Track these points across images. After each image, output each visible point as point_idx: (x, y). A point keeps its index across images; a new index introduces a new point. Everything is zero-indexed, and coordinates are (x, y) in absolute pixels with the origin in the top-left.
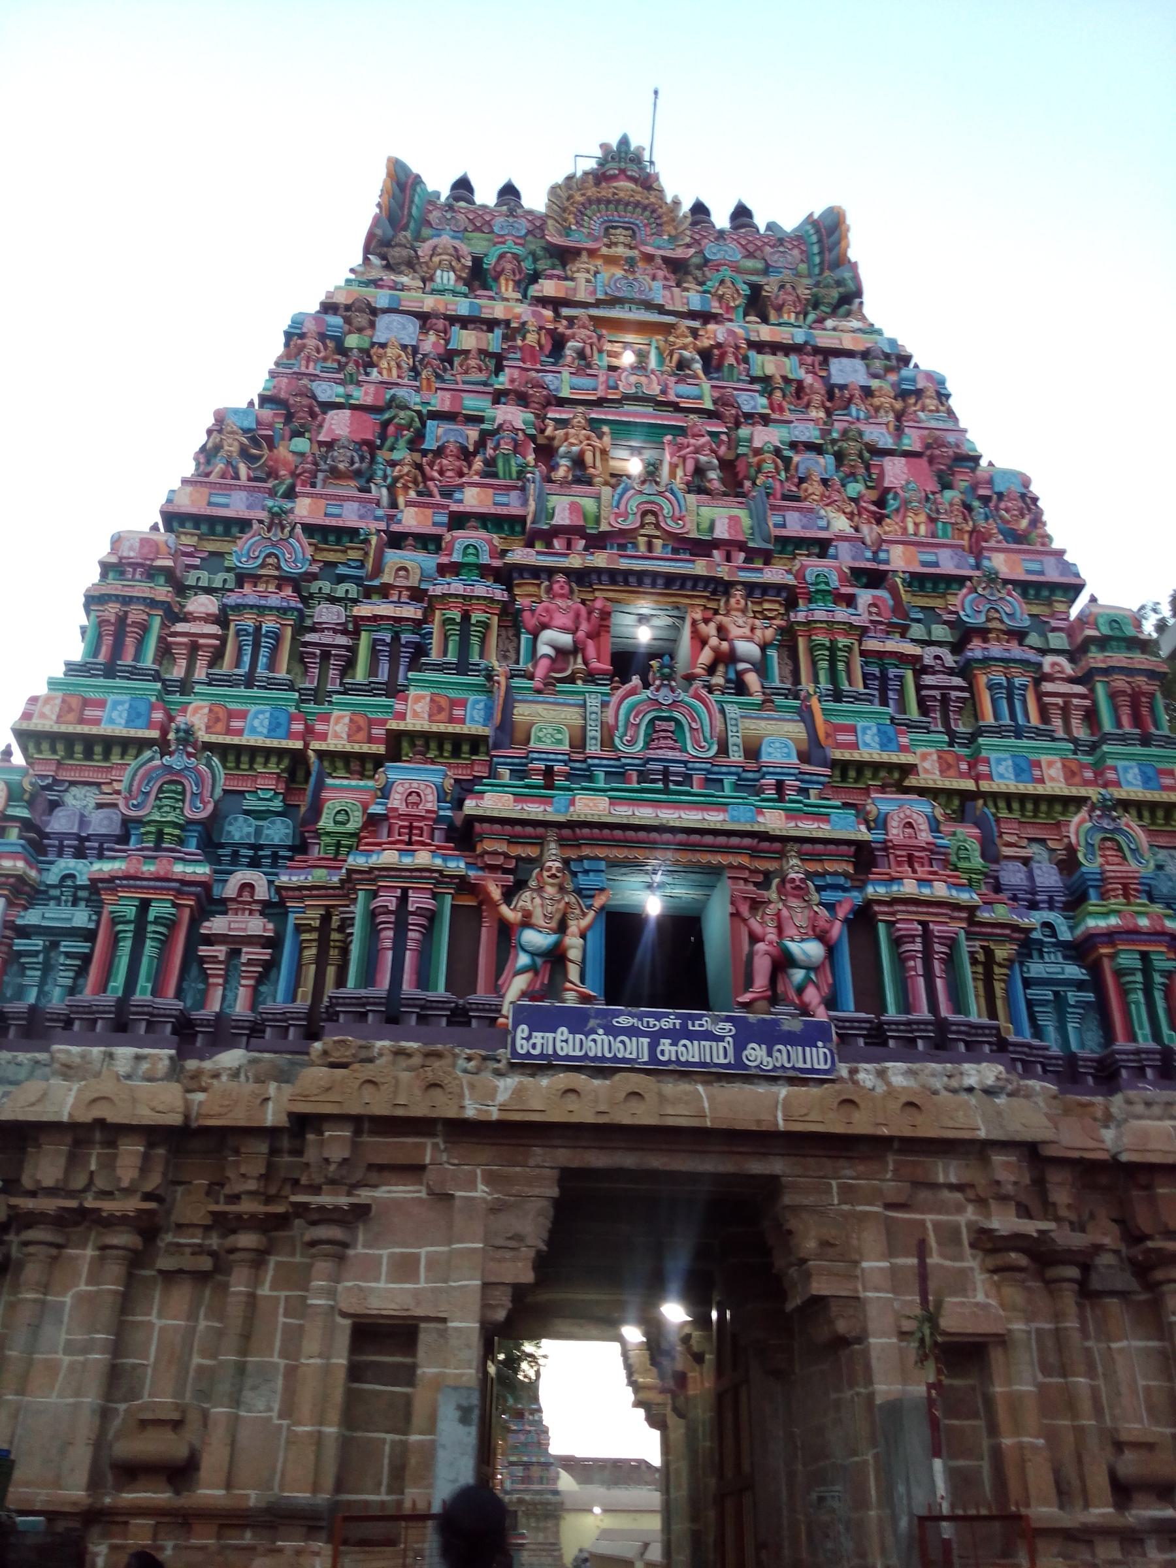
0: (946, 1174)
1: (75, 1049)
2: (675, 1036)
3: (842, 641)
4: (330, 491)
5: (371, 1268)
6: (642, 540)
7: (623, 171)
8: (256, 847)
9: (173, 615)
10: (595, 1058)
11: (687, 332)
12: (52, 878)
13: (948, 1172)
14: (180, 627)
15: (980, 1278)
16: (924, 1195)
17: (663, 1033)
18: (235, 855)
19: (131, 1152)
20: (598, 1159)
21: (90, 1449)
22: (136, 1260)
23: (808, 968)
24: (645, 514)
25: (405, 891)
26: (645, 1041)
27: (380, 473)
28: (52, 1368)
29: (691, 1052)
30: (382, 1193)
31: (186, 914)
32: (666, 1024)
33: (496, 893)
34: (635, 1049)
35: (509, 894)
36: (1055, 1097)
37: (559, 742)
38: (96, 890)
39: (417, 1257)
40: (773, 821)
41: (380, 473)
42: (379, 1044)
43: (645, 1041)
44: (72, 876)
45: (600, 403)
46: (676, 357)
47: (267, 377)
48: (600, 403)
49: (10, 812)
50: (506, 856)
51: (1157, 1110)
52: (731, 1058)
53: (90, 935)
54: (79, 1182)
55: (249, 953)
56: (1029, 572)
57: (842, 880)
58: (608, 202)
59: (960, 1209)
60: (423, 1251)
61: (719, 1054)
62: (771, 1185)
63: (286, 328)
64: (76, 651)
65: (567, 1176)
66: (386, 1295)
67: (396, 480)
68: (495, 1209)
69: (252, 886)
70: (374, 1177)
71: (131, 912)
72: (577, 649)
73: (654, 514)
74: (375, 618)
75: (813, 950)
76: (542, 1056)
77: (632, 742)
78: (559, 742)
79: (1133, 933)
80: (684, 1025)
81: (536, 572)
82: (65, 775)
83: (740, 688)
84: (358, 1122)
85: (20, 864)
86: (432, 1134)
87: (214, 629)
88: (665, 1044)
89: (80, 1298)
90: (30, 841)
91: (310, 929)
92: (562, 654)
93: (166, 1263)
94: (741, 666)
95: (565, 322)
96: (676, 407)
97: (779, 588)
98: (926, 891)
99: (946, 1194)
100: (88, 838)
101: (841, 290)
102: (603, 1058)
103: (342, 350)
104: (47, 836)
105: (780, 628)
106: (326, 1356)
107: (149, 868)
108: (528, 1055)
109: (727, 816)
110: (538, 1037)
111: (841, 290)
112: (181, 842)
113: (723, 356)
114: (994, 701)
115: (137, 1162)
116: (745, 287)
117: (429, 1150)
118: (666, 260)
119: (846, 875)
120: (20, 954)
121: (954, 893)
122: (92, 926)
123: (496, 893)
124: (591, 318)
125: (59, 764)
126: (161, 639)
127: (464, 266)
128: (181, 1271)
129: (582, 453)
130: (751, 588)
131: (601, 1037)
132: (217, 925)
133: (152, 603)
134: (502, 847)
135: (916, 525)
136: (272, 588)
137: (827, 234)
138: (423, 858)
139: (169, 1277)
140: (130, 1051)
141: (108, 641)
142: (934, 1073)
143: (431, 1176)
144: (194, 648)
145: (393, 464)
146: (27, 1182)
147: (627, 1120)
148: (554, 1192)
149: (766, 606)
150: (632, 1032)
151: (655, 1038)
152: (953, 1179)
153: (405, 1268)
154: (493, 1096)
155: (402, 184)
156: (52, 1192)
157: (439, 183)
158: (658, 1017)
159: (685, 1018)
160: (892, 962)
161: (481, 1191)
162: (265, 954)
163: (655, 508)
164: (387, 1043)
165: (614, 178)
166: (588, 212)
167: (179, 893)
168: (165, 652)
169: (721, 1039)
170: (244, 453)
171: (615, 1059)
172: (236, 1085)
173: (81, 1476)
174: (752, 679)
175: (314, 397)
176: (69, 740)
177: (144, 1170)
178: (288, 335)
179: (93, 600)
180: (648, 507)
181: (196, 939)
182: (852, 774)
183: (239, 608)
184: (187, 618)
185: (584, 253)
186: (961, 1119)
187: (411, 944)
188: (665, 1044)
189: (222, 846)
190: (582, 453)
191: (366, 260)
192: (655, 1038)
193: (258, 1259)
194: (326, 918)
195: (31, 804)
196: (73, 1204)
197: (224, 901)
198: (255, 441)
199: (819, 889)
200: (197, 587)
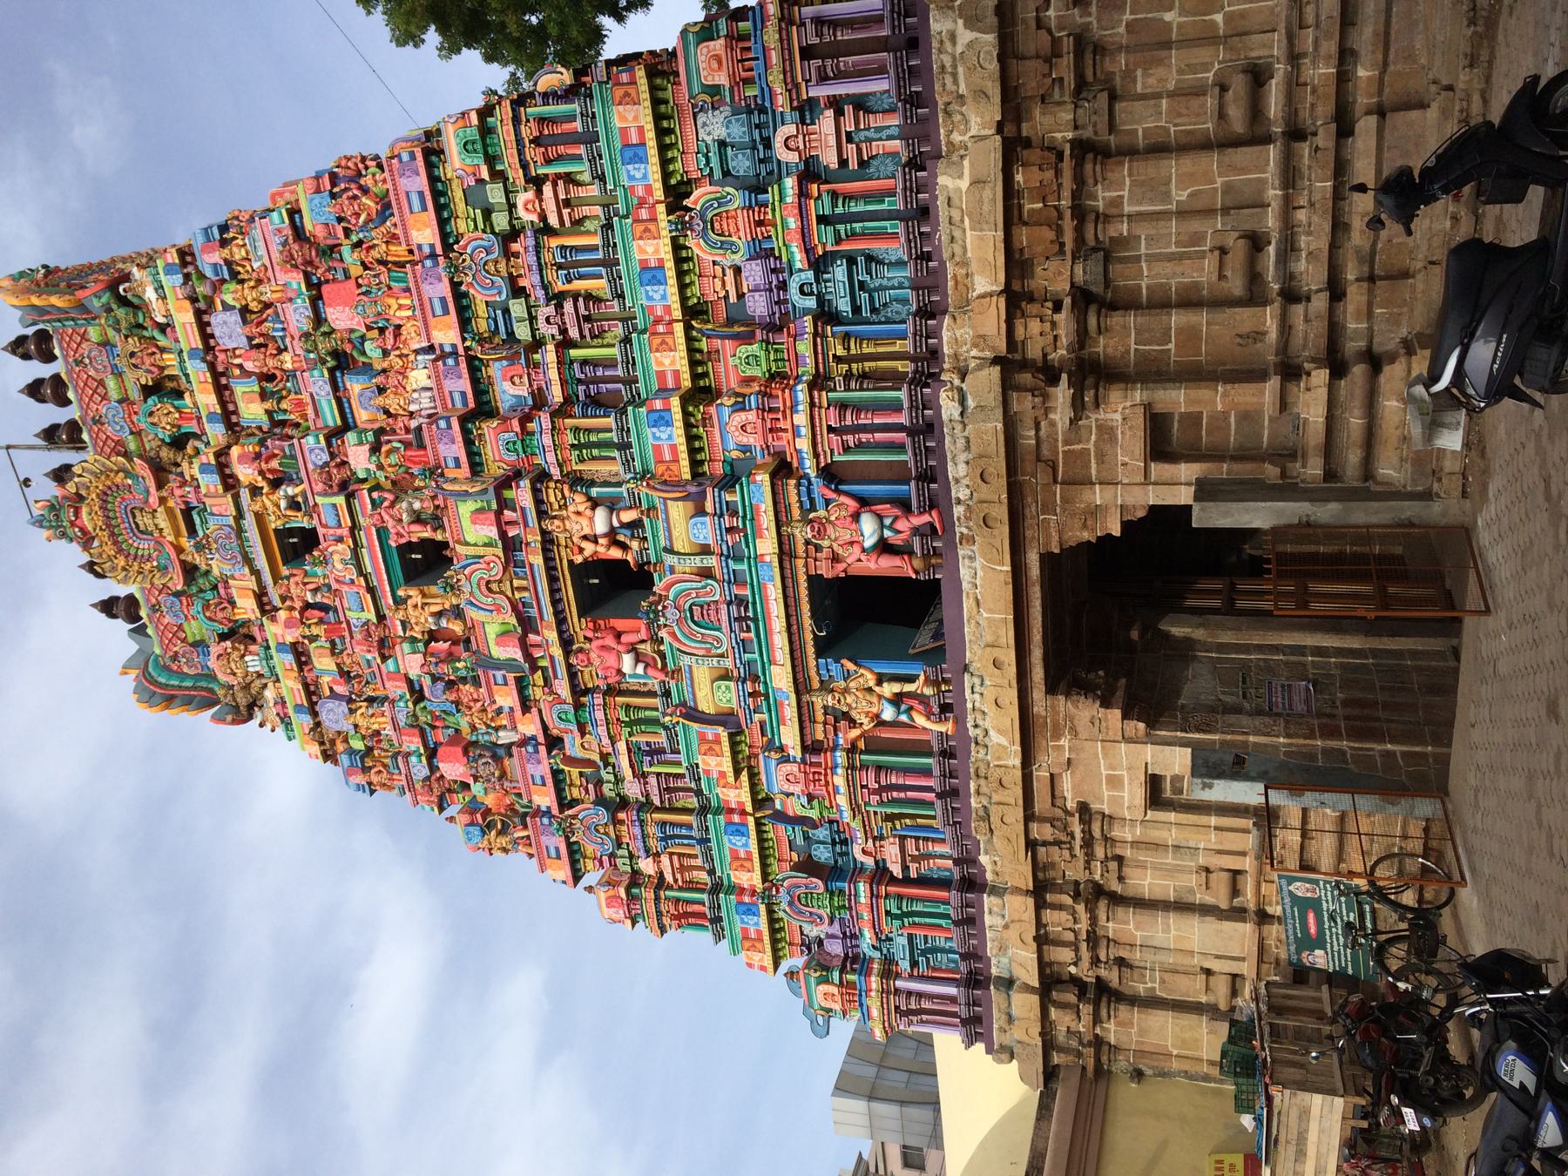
0: (1029, 438)
1: (989, 945)
3: (570, 439)
5: (1114, 800)
6: (517, 595)
7: (73, 524)
8: (834, 843)
12: (877, 955)
13: (1028, 437)
15: (1102, 416)
16: (1045, 452)
18: (842, 854)
19: (1049, 915)
20: (1038, 674)
23: (882, 526)
24: (490, 590)
27: (486, 738)
28: (1177, 938)
30: (1068, 795)
31: (891, 889)
33: (855, 733)
35: (853, 723)
36: (954, 318)
37: (728, 688)
39: (1108, 776)
40: (767, 546)
41: (486, 738)
42: (973, 804)
46: (289, 513)
49: (837, 981)
50: (825, 723)
51: (957, 234)
55: (910, 846)
56: (424, 209)
57: (803, 489)
58: (113, 534)
59: (1053, 424)
60: (1104, 772)
62: (1046, 559)
65: (1051, 689)
66: (1133, 795)
67: (488, 726)
68: (1074, 732)
70: (1059, 802)
72: (632, 649)
73: (488, 582)
74: (632, 766)
75: (868, 525)
77: (718, 640)
78: (728, 688)
79: (804, 233)
81: (572, 675)
82: (798, 940)
83: (635, 525)
84: (1029, 817)
85: (873, 979)
86: (1031, 773)
89: (1137, 929)
91: (837, 232)
92: (638, 658)
94: (616, 524)
97: (536, 492)
98: (803, 431)
99: (1042, 433)
100: (844, 934)
101: (114, 306)
104: (846, 955)
105: (571, 490)
106: (1170, 826)
107: (866, 916)
109: (770, 586)
111: (114, 306)
112: (841, 892)
113: (272, 471)
114: (581, 277)
115: (1056, 913)
116: (150, 401)
117: (1040, 774)
118: (160, 486)
119: (798, 485)
120: (822, 682)
121: (801, 408)
123: (855, 733)
125: (790, 944)
126: (681, 889)
127: (234, 648)
129: (433, 614)
130: (542, 514)
134: (820, 727)
135: (400, 307)
138: (839, 780)
139: (1121, 879)
140: (987, 916)
142: (953, 444)
143: (1055, 771)
144: (683, 869)
145: (474, 728)
147: (1014, 669)
148: (1062, 698)
149: (552, 499)
152: (1033, 433)
153: (1114, 782)
154: (1005, 748)
160: (864, 453)
161: (1064, 742)
163: (483, 583)
164: (972, 800)
165: (82, 530)
166: (132, 552)
167: (878, 897)
170: (503, 832)
172: (1001, 859)
173: (1239, 925)
174: (628, 516)
175: (428, 778)
176: (774, 942)
180: (484, 588)
181: (907, 881)
182: (697, 444)
184: (661, 875)
186: (990, 438)
187: (901, 781)
190: (433, 614)
195: (827, 969)
197: (877, 862)
198: (490, 826)
199: (813, 508)
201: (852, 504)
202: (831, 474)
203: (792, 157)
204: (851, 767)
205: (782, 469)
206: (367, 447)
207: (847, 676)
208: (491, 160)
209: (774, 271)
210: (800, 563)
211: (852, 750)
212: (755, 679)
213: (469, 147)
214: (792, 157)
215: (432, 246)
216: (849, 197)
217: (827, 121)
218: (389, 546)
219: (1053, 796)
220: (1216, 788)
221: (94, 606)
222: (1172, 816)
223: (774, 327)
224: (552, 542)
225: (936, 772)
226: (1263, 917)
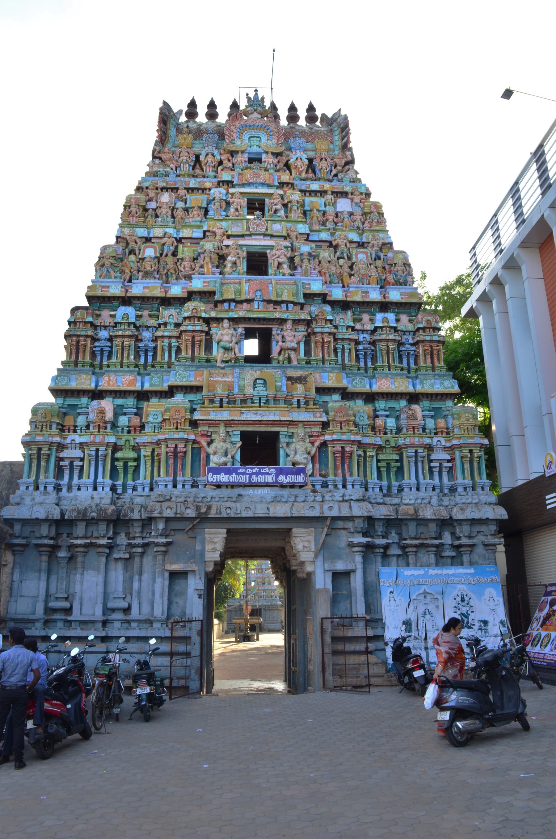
2: (257, 474)
4: (144, 281)
9: (94, 339)
10: (232, 482)
11: (278, 196)
14: (97, 344)
17: (253, 474)
21: (478, 518)
22: (108, 556)
25: (176, 445)
26: (248, 476)
29: (262, 479)
32: (254, 471)
34: (244, 479)
35: (209, 444)
38: (82, 446)
40: (296, 416)
43: (248, 476)
44: (74, 440)
45: (243, 236)
47: (118, 227)
48: (243, 236)
52: (274, 480)
53: (82, 459)
54: (89, 534)
61: (270, 479)
63: (124, 203)
64: (63, 356)
69: (129, 441)
71: (93, 453)
76: (216, 482)
80: (260, 471)
87: (109, 344)
88: (254, 477)
90: (60, 429)
91: (148, 456)
93: (116, 556)
95: (230, 196)
96: (272, 236)
102: (235, 482)
103: (146, 210)
108: (212, 482)
110: (215, 476)
122: (82, 456)
123: (204, 444)
124: (241, 193)
126: (91, 348)
128: (120, 558)
131: (234, 475)
132: (119, 455)
133: (87, 336)
134: (206, 429)
136: (126, 327)
137: (339, 126)
139: (116, 559)
141: (74, 351)
146: (75, 535)
150: (244, 474)
151: (251, 475)
155: (166, 116)
156: (82, 538)
157: (180, 105)
158: (252, 469)
159: (260, 469)
162: (135, 464)
168: (93, 355)
169: (271, 474)
171: (238, 482)
177: (107, 531)
178: (125, 207)
179: (67, 337)
181: (114, 460)
183: (116, 336)
185: (240, 152)
188: (254, 477)
189: (118, 427)
191: (153, 161)
192: (251, 475)
193: (142, 554)
194: (153, 452)
196: (88, 541)
200: (101, 326)
201: (313, 452)
202: (324, 444)
203: (68, 441)
204: (187, 441)
205: (325, 425)
206: (310, 251)
207: (233, 443)
208: (424, 329)
209: (135, 429)
210: (286, 429)
211: (194, 442)
212: (228, 403)
213: (195, 310)
214: (435, 443)
215: (388, 297)
216: (423, 462)
217: (446, 456)
218: (268, 249)
219: (174, 530)
220: (199, 600)
221: (340, 110)
222: (167, 582)
223: (373, 428)
224: (281, 323)
225: (28, 480)
226: (105, 623)
